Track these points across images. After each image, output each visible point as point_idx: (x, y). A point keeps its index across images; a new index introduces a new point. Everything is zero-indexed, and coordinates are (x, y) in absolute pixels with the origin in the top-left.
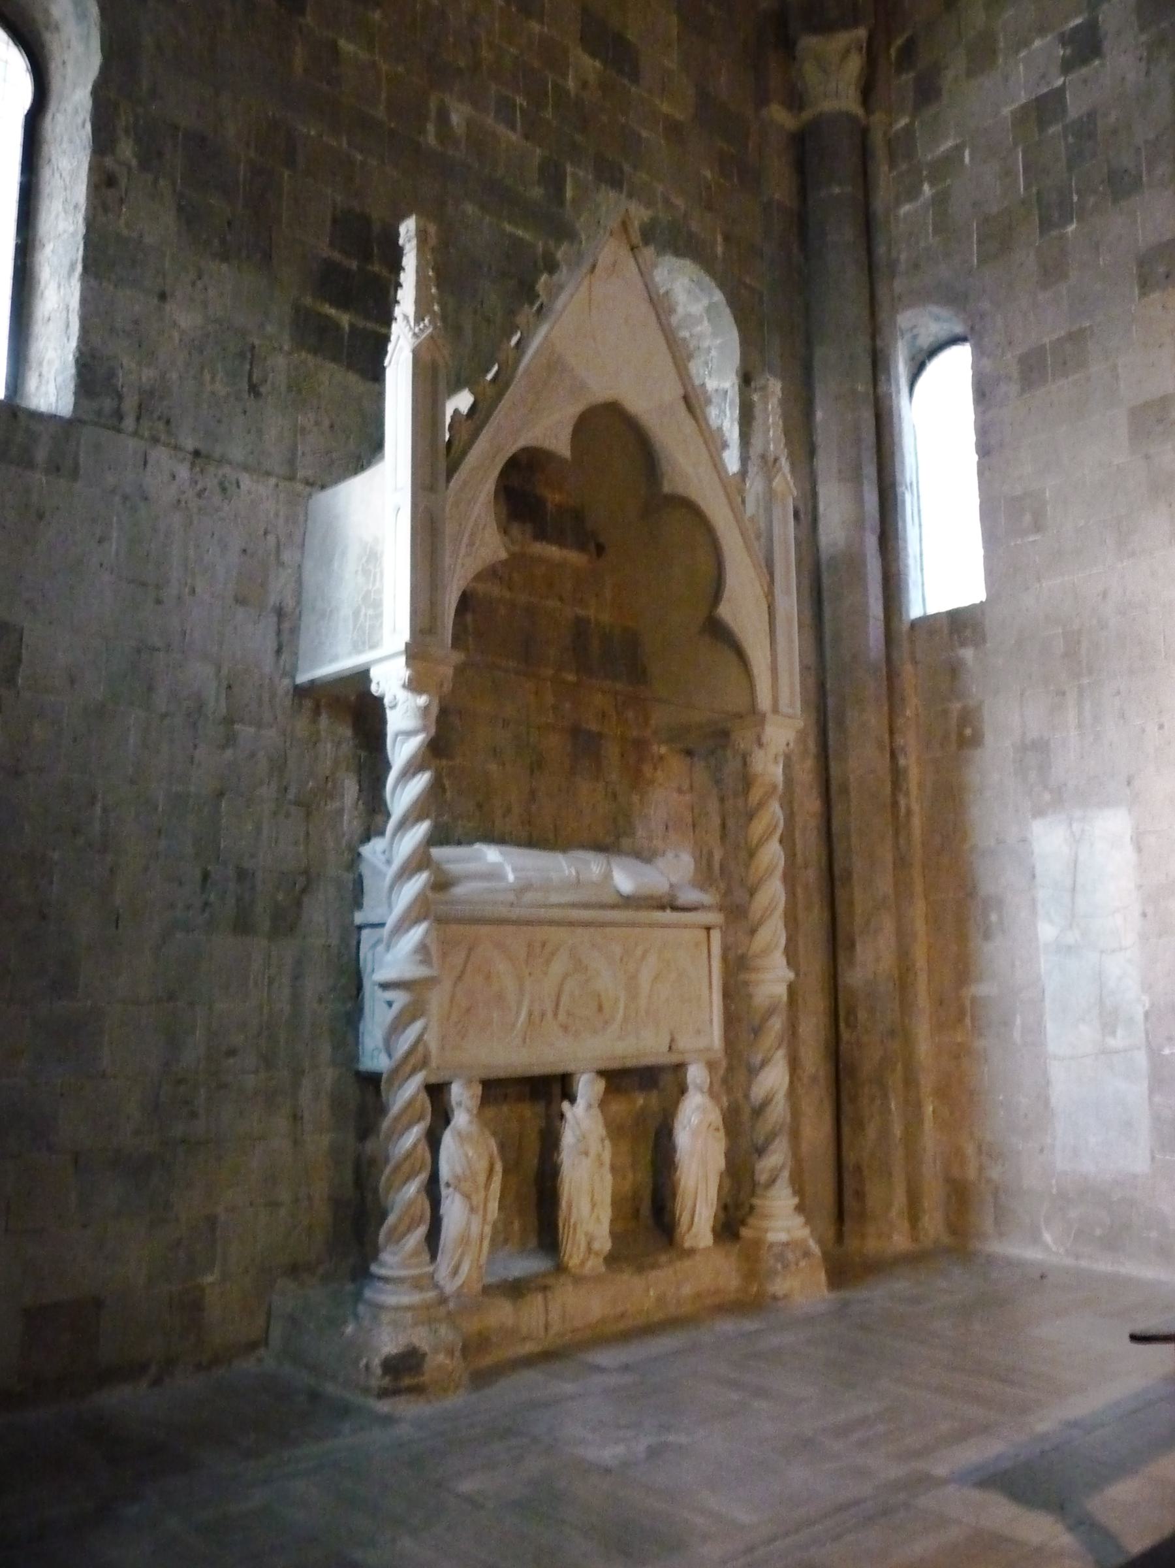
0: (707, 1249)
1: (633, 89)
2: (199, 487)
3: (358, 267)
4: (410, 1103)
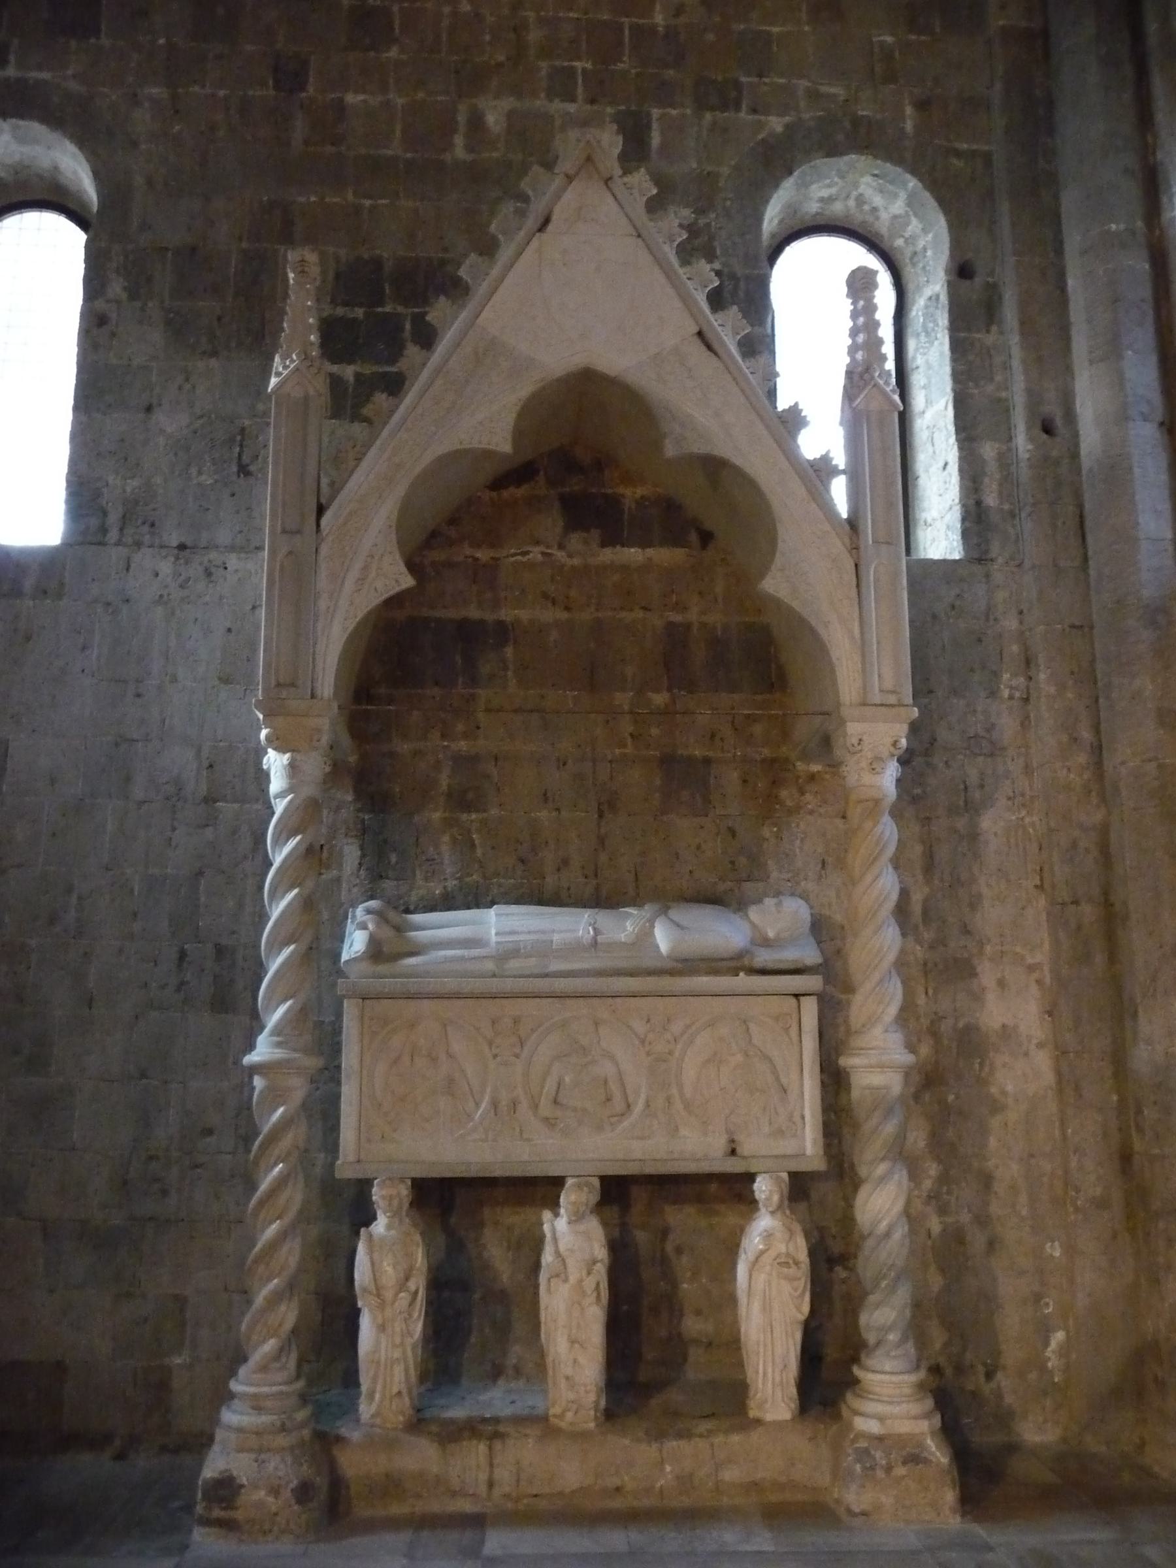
0: (779, 1425)
2: (182, 578)
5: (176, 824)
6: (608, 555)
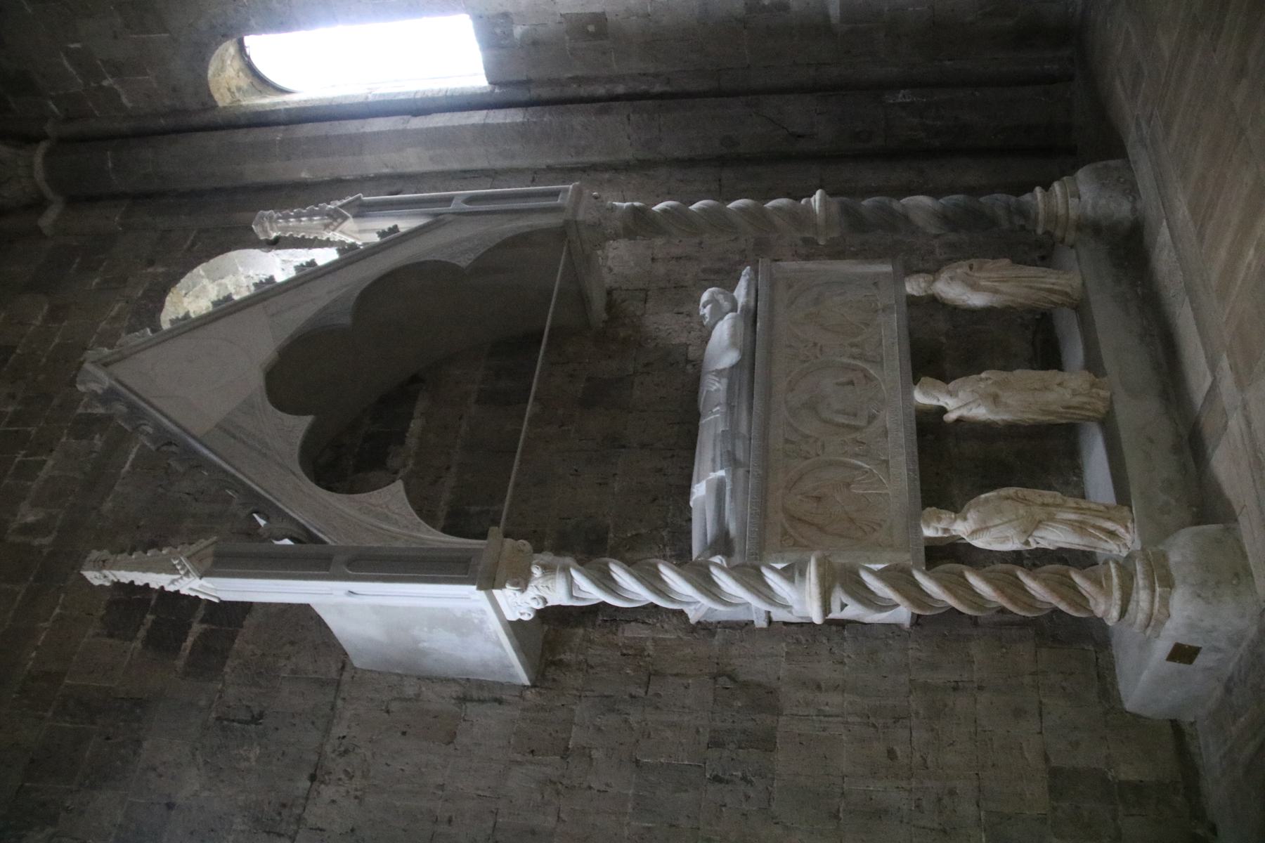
1: (18, 351)
2: (343, 776)
3: (151, 613)
4: (947, 588)
5: (585, 785)
6: (412, 442)
